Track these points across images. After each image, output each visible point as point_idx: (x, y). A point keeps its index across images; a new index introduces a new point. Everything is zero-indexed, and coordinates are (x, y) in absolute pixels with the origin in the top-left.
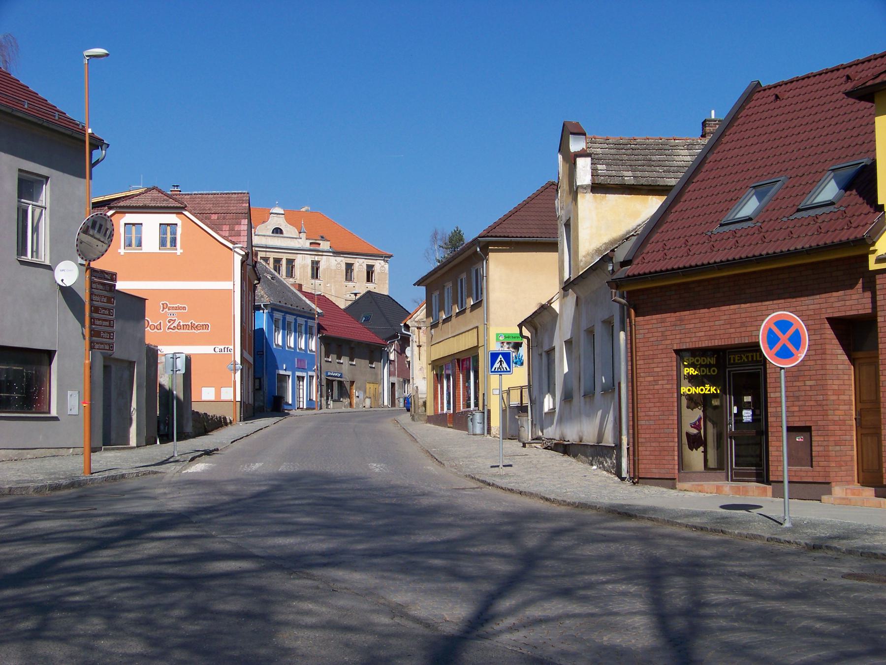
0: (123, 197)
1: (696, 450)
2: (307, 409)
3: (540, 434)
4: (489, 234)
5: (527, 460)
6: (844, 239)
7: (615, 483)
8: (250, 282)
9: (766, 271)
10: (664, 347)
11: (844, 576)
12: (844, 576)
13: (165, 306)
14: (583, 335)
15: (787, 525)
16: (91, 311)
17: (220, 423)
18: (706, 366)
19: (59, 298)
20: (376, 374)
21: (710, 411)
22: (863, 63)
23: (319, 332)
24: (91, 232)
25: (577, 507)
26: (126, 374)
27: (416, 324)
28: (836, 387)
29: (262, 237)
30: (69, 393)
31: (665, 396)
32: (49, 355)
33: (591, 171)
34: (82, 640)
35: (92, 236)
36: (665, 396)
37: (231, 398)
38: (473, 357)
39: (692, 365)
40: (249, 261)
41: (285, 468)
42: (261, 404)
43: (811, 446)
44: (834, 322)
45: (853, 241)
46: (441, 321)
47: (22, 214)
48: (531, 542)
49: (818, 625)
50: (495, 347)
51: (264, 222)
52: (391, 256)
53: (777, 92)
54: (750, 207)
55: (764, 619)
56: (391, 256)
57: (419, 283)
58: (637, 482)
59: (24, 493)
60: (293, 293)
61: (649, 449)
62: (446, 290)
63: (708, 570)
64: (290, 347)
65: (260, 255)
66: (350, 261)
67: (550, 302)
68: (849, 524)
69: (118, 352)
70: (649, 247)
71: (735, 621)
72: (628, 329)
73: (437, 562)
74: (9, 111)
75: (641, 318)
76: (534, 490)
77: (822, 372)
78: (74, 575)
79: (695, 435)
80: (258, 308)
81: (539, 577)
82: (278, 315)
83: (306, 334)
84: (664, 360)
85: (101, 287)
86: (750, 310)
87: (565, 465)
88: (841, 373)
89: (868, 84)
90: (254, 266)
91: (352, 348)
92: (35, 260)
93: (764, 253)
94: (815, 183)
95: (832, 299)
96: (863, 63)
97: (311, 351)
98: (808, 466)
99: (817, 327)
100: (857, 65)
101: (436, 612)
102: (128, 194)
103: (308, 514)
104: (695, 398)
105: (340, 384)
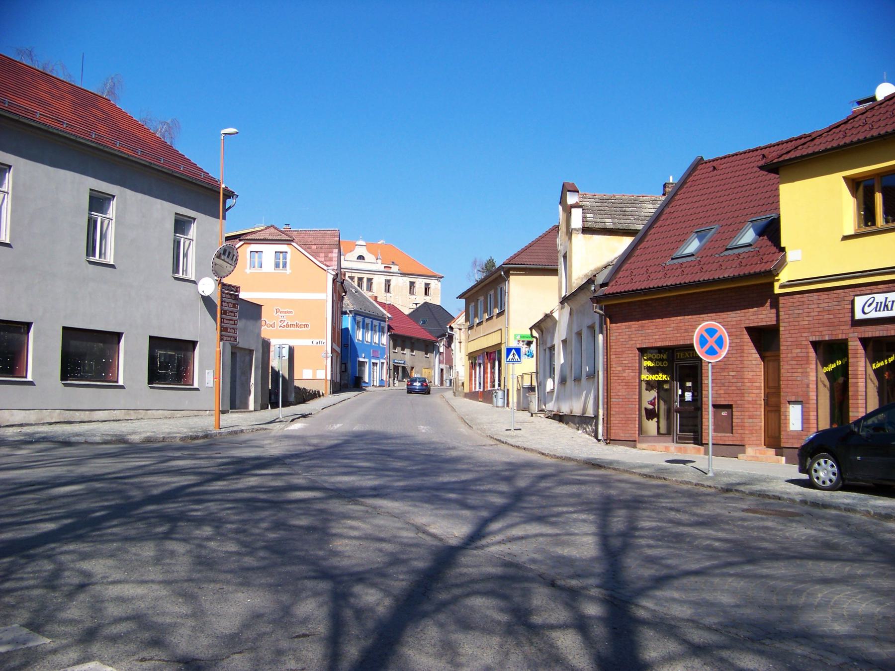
0: (250, 233)
1: (652, 420)
2: (379, 386)
3: (544, 407)
4: (510, 263)
5: (532, 426)
6: (757, 270)
7: (593, 443)
8: (339, 294)
9: (703, 292)
10: (630, 346)
11: (744, 510)
12: (744, 510)
13: (278, 311)
14: (574, 336)
15: (710, 474)
16: (221, 314)
17: (315, 395)
18: (660, 360)
19: (201, 304)
20: (430, 362)
21: (662, 393)
22: (774, 146)
23: (388, 331)
24: (223, 257)
25: (564, 459)
26: (247, 358)
27: (458, 327)
28: (750, 377)
29: (349, 262)
30: (207, 371)
31: (631, 381)
32: (194, 344)
33: (581, 218)
34: (196, 542)
35: (223, 260)
36: (631, 381)
37: (324, 377)
38: (498, 351)
39: (650, 359)
40: (339, 279)
41: (358, 428)
42: (346, 382)
43: (732, 419)
44: (750, 330)
45: (763, 272)
46: (475, 325)
47: (177, 244)
48: (522, 483)
49: (717, 544)
50: (513, 344)
51: (351, 251)
52: (443, 277)
53: (715, 165)
54: (693, 246)
55: (678, 538)
56: (443, 277)
57: (460, 297)
58: (609, 443)
59: (173, 441)
60: (371, 303)
61: (618, 419)
62: (479, 301)
63: (648, 505)
64: (367, 342)
65: (347, 275)
66: (412, 280)
67: (552, 313)
68: (754, 475)
69: (242, 343)
70: (620, 274)
71: (660, 540)
72: (605, 332)
73: (452, 496)
74: (170, 172)
75: (614, 325)
76: (533, 447)
77: (741, 366)
78: (197, 498)
79: (651, 410)
80: (345, 313)
81: (526, 508)
82: (359, 318)
83: (379, 332)
84: (630, 355)
85: (229, 296)
86: (692, 320)
87: (559, 430)
88: (754, 366)
89: (774, 161)
90: (342, 283)
91: (413, 343)
92: (184, 277)
93: (701, 279)
94: (738, 230)
95: (749, 314)
96: (774, 146)
97: (383, 344)
98: (729, 433)
99: (738, 333)
100: (770, 147)
101: (449, 530)
102: (253, 230)
103: (368, 460)
104: (652, 383)
105: (404, 368)
